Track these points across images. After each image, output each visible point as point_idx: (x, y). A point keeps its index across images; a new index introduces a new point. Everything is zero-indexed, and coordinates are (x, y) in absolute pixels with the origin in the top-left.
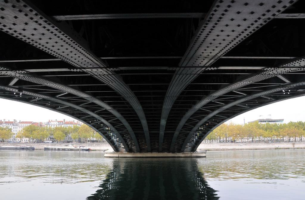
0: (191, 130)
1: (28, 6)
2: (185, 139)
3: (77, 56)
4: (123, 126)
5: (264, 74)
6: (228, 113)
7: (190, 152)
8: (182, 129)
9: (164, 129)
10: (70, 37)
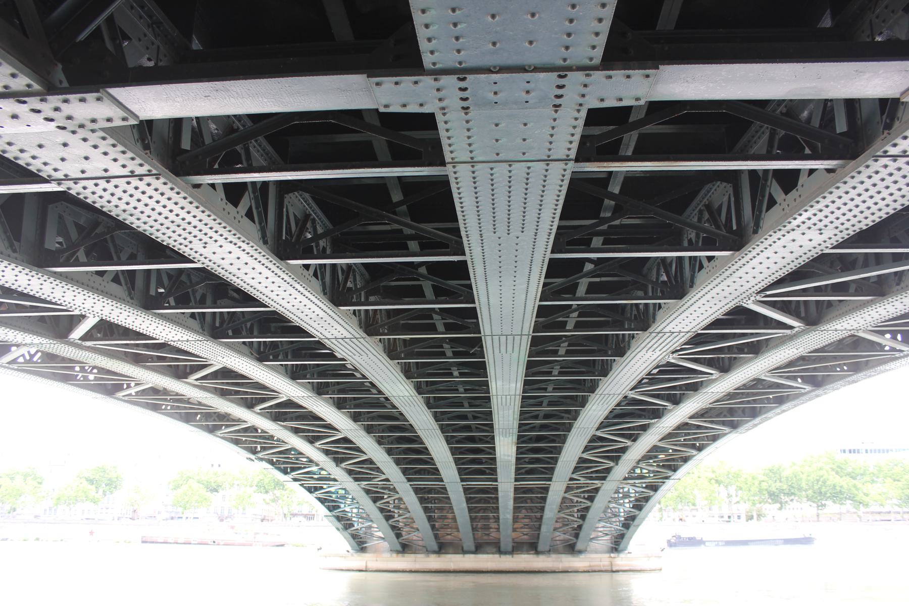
0: (604, 478)
1: (20, 74)
2: (587, 509)
3: (263, 285)
4: (370, 461)
5: (825, 330)
6: (731, 412)
7: (607, 555)
8: (573, 473)
9: (513, 475)
10: (143, 160)
